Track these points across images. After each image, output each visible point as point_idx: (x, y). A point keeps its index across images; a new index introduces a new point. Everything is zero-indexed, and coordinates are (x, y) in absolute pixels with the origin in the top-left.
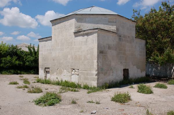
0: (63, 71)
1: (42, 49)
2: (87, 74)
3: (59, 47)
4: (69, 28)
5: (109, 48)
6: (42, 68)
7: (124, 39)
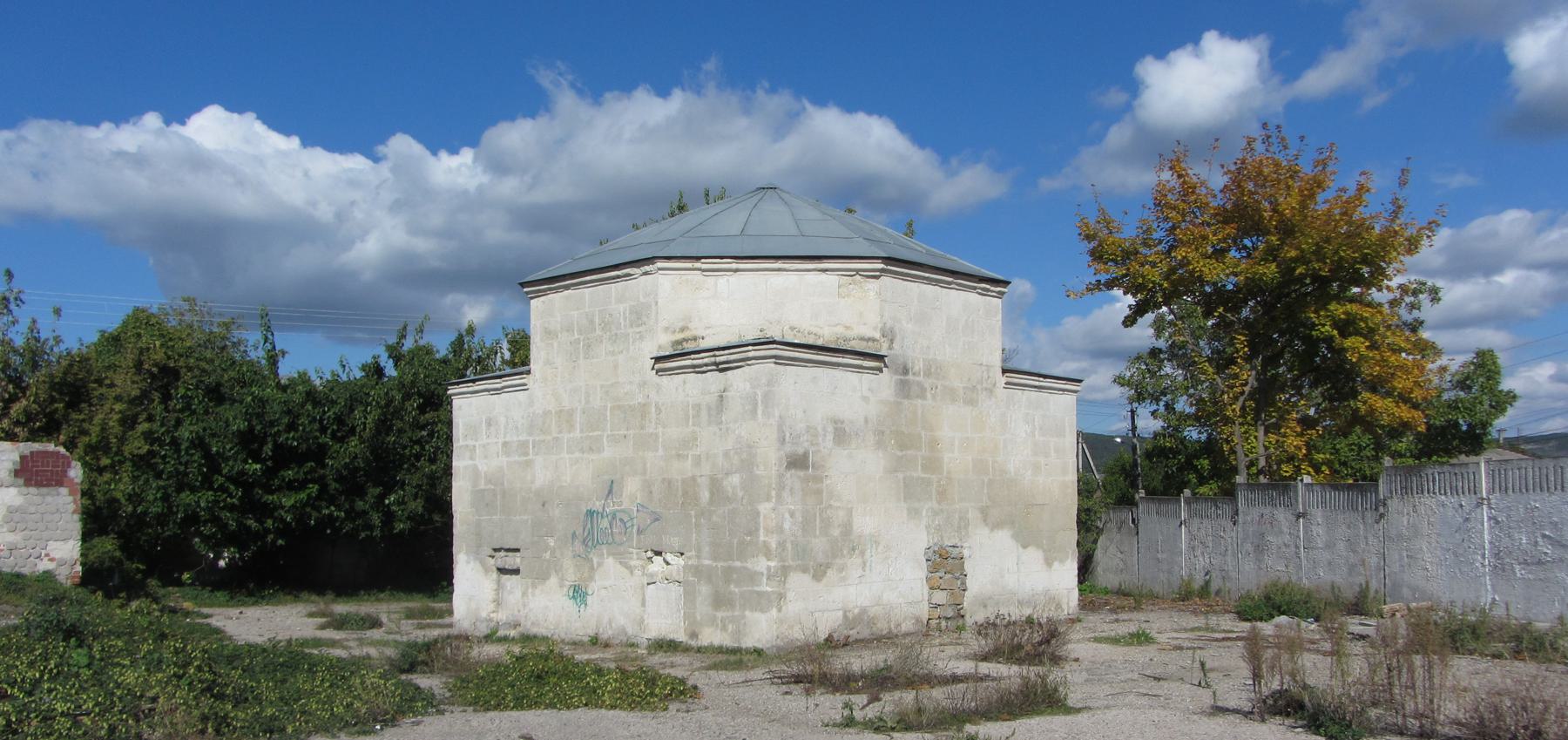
0: (600, 565)
1: (470, 443)
2: (729, 571)
3: (577, 434)
4: (630, 331)
5: (841, 434)
6: (475, 552)
7: (927, 383)
